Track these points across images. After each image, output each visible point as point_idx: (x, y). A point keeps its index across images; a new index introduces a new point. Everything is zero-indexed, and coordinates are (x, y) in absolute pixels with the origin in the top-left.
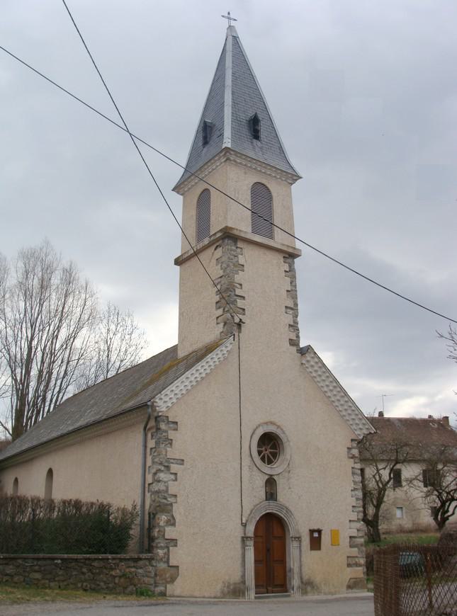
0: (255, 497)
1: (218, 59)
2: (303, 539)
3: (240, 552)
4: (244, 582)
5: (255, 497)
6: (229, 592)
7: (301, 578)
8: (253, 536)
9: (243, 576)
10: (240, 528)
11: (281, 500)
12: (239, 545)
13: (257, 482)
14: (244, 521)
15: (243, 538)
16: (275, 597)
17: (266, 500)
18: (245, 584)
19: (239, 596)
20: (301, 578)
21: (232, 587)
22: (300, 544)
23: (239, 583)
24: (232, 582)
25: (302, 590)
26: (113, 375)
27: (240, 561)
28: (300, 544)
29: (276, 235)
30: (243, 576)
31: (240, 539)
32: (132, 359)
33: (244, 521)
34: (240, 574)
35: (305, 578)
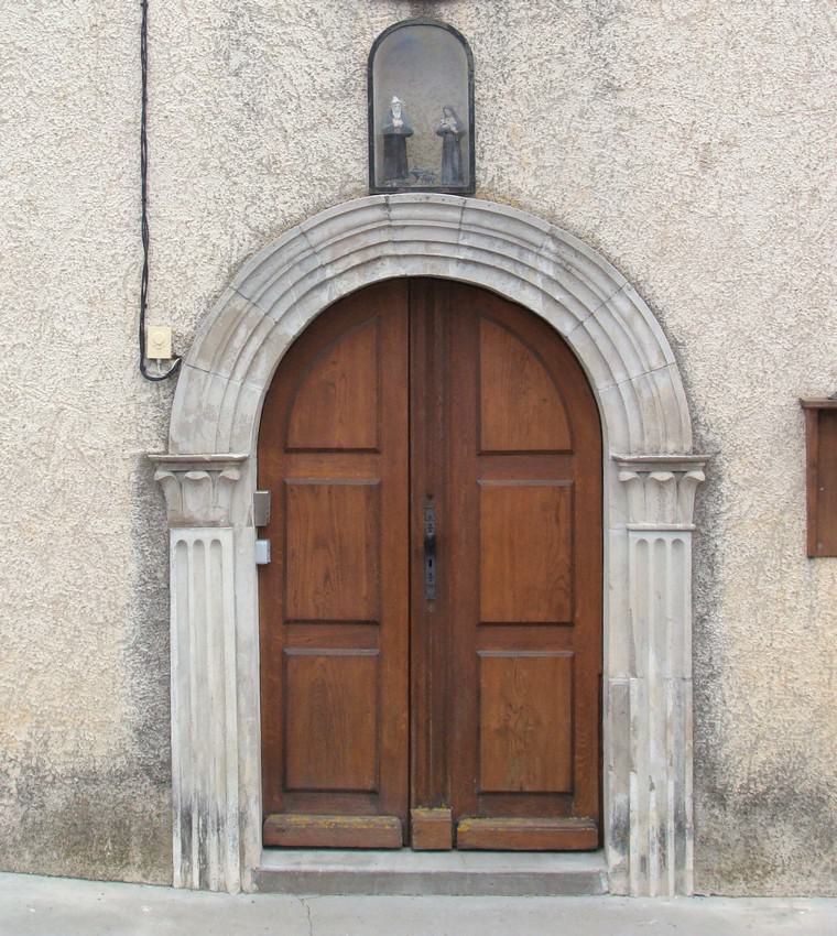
0: (269, 167)
1: (532, 308)
2: (734, 472)
3: (125, 562)
4: (160, 774)
5: (269, 167)
6: (32, 832)
7: (705, 766)
8: (247, 448)
9: (155, 727)
10: (125, 391)
11: (524, 182)
12: (118, 521)
13: (289, 60)
14: (160, 347)
15: (149, 464)
16: (436, 884)
17: (374, 190)
18: (165, 782)
19: (122, 858)
20: (705, 766)
21: (56, 799)
22: (701, 514)
23: (119, 777)
24: (58, 760)
25: (703, 842)
26: (231, 477)
27: (126, 629)
28: (701, 514)
29: (611, 623)
30: (155, 727)
31: (126, 474)
32: (617, 815)
33: (160, 347)
34: (124, 711)
35: (745, 759)
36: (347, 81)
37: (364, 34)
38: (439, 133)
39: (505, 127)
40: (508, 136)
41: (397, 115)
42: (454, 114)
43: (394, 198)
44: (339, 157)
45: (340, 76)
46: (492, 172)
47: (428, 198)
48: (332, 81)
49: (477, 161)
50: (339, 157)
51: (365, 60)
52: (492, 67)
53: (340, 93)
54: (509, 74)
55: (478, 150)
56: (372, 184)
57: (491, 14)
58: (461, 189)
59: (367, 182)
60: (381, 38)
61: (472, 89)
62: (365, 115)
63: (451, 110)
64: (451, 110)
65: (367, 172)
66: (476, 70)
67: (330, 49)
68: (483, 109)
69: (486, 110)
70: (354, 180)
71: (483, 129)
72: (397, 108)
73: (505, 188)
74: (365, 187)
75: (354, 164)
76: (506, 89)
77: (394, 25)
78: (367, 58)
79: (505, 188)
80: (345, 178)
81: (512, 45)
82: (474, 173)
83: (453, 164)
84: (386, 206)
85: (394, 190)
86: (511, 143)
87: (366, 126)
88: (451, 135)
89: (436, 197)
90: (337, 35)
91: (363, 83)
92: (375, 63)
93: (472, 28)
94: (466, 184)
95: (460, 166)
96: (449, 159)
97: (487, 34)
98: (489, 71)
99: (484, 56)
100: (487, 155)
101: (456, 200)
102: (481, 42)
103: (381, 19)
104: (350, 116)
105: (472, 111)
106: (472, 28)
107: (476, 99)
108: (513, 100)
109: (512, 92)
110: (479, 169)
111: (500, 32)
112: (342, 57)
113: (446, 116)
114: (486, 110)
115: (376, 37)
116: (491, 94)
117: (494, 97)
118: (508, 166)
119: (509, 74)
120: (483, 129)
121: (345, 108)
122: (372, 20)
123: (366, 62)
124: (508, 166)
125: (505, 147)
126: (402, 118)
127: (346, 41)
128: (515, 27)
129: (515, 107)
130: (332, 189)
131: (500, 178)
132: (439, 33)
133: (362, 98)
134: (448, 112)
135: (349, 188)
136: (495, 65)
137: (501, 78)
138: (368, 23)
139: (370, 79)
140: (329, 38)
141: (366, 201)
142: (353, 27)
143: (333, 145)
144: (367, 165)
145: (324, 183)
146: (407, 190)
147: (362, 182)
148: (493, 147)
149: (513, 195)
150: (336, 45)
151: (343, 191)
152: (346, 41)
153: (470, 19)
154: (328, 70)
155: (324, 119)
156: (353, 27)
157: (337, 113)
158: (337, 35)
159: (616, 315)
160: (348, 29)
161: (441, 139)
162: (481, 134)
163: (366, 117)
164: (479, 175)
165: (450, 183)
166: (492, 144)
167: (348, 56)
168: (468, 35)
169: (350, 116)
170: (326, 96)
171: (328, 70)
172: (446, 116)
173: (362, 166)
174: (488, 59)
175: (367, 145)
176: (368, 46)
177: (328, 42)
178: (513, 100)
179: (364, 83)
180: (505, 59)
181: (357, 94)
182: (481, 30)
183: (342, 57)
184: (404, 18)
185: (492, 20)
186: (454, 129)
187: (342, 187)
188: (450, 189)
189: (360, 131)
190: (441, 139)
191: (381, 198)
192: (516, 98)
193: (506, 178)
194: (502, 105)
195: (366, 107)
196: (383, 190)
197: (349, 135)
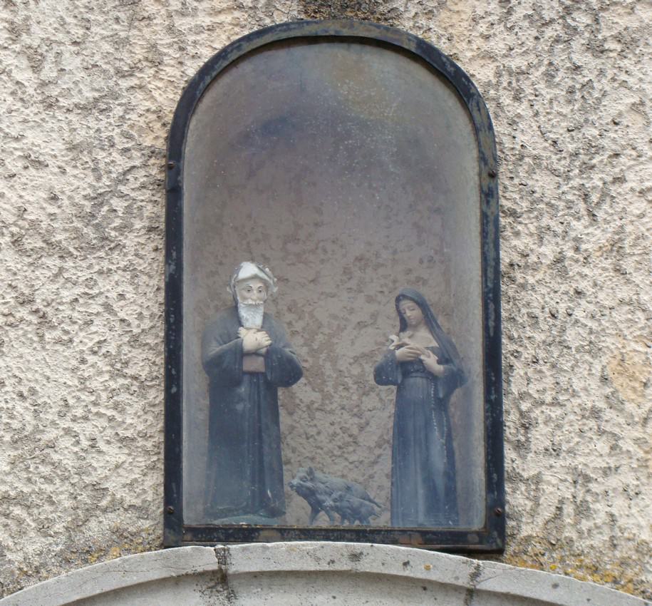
1: (269, 41)
36: (98, 200)
37: (157, 64)
38: (382, 376)
39: (593, 350)
40: (604, 380)
41: (252, 318)
42: (429, 321)
43: (244, 557)
44: (68, 431)
45: (78, 184)
46: (556, 488)
47: (355, 557)
48: (54, 198)
49: (509, 453)
50: (68, 431)
51: (157, 138)
52: (554, 172)
53: (78, 235)
54: (605, 195)
55: (511, 421)
56: (172, 516)
57: (547, 15)
58: (461, 536)
59: (158, 510)
60: (192, 96)
61: (491, 235)
62: (154, 302)
63: (422, 304)
64: (422, 304)
65: (157, 478)
66: (503, 179)
67: (50, 105)
68: (525, 296)
69: (536, 299)
70: (116, 505)
71: (527, 354)
72: (254, 297)
73: (599, 540)
74: (151, 525)
75: (115, 454)
76: (596, 237)
77: (247, 38)
78: (163, 134)
79: (599, 540)
80: (84, 497)
81: (611, 108)
82: (501, 492)
83: (426, 465)
84: (220, 579)
85: (247, 535)
86: (614, 402)
87: (156, 338)
88: (418, 382)
89: (381, 557)
90: (72, 62)
91: (149, 210)
92: (189, 149)
93: (489, 56)
94: (476, 521)
95: (450, 474)
96: (440, 482)
97: (536, 74)
98: (543, 183)
99: (527, 137)
100: (540, 437)
101: (451, 567)
102: (517, 98)
103: (207, 21)
104: (108, 307)
105: (492, 297)
106: (489, 56)
107: (503, 268)
108: (618, 270)
109: (615, 247)
110: (517, 478)
111: (577, 68)
112: (84, 129)
113: (404, 325)
114: (536, 299)
115: (192, 70)
116: (548, 251)
117: (559, 260)
118: (607, 471)
119: (605, 195)
120: (527, 354)
121: (90, 283)
122: (182, 24)
123: (161, 144)
124: (607, 471)
125: (595, 413)
126: (266, 326)
127: (100, 83)
128: (622, 55)
129: (625, 293)
130: (43, 529)
131: (583, 510)
132: (384, 66)
133: (148, 252)
134: (412, 313)
135: (97, 529)
136: (561, 167)
137: (582, 206)
138: (171, 29)
139: (173, 192)
140: (48, 72)
141: (152, 564)
142: (120, 43)
143: (50, 395)
144: (158, 459)
145: (17, 511)
146: (285, 533)
147: (142, 511)
148: (556, 412)
149: (623, 563)
150: (67, 93)
151: (80, 540)
152: (100, 83)
153: (482, 27)
154: (39, 164)
155: (23, 312)
156: (120, 43)
157: (67, 295)
158: (72, 62)
159: (491, 323)
160: (107, 47)
161: (388, 393)
162: (519, 370)
163: (158, 310)
164: (516, 499)
165: (421, 518)
166: (555, 403)
167: (106, 125)
168: (481, 74)
169: (108, 307)
170: (33, 242)
171: (39, 164)
172: (404, 325)
173: (142, 461)
174: (538, 147)
175: (157, 395)
176: (168, 100)
177: (43, 84)
178: (618, 270)
179: (153, 208)
180: (593, 148)
181: (130, 241)
182: (517, 63)
183: (84, 129)
184: (280, 19)
185: (549, 32)
186: (431, 361)
187: (77, 526)
188: (424, 533)
189: (138, 354)
190: (388, 393)
191: (203, 557)
192: (628, 265)
193: (600, 507)
194: (583, 285)
195: (158, 281)
196: (205, 535)
197: (103, 365)
